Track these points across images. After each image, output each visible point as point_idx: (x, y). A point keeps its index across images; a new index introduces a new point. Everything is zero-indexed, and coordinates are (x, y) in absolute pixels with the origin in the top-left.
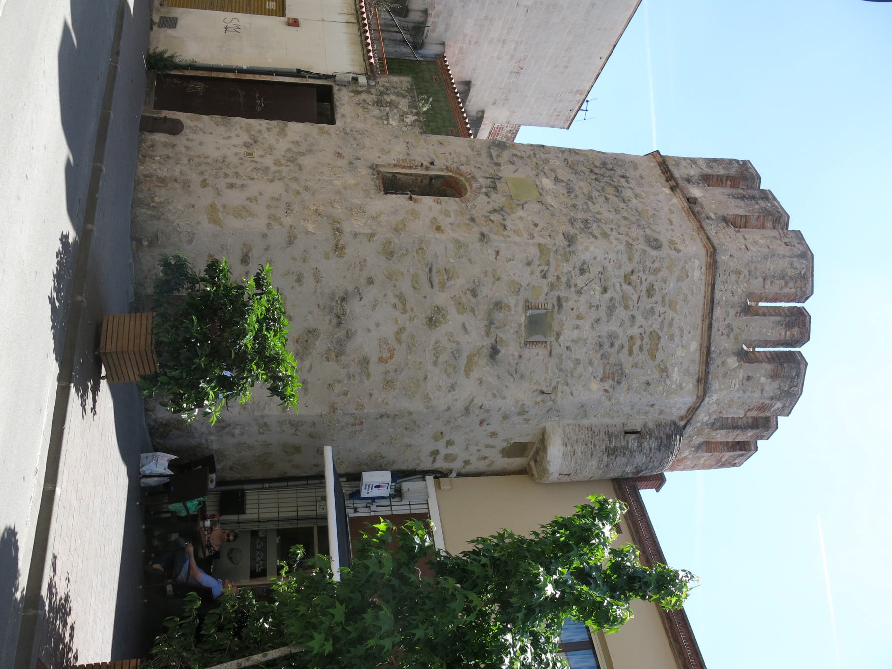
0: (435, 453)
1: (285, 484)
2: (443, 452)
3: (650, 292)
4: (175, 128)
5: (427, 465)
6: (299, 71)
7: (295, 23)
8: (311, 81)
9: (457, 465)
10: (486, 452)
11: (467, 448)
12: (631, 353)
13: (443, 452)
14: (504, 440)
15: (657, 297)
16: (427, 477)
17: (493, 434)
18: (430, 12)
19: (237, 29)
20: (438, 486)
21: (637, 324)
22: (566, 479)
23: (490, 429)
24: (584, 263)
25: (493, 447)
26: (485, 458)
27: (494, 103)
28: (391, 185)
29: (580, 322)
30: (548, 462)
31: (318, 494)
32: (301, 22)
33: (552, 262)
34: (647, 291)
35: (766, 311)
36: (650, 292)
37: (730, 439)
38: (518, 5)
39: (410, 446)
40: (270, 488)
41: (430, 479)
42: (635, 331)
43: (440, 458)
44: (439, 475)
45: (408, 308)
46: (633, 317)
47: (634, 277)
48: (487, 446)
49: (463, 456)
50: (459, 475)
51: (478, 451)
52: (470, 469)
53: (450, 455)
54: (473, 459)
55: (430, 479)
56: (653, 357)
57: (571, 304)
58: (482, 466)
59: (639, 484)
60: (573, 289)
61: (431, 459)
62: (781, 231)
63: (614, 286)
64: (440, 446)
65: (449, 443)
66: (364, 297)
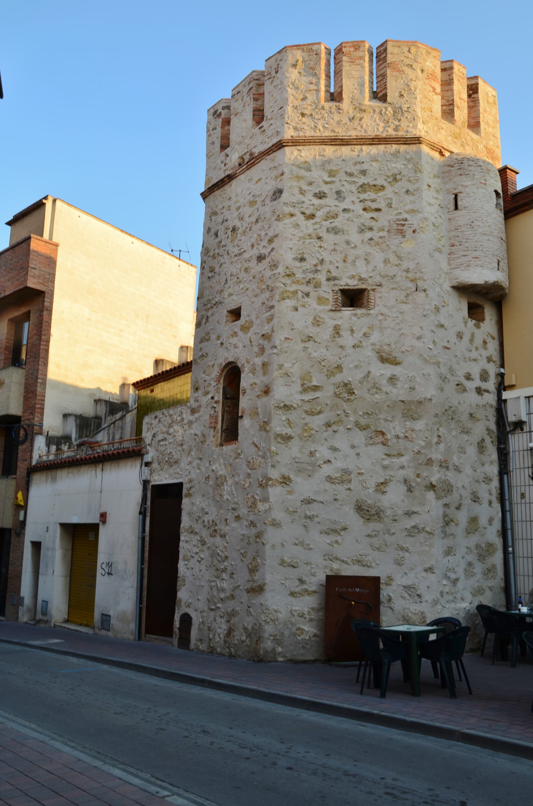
0: (479, 391)
1: (509, 532)
2: (477, 383)
3: (321, 196)
4: (186, 619)
5: (491, 399)
6: (140, 513)
7: (103, 516)
8: (149, 503)
9: (492, 370)
10: (478, 341)
11: (474, 360)
12: (378, 210)
13: (477, 383)
14: (466, 323)
15: (325, 188)
16: (503, 398)
17: (460, 336)
18: (97, 398)
19: (110, 565)
20: (512, 387)
21: (352, 207)
22: (504, 265)
23: (454, 339)
24: (295, 259)
25: (473, 335)
26: (485, 342)
27: (175, 337)
28: (231, 433)
29: (350, 259)
30: (486, 282)
31: (519, 501)
32: (102, 510)
33: (294, 287)
34: (320, 198)
35: (338, 86)
36: (321, 196)
37: (465, 105)
38: (89, 320)
39: (471, 415)
40: (513, 546)
41: (505, 395)
42: (358, 208)
43: (485, 386)
44: (502, 386)
45: (337, 419)
46: (345, 210)
47: (308, 212)
48: (472, 340)
49: (483, 364)
50: (502, 366)
51: (477, 349)
52: (496, 357)
53: (481, 376)
54: (486, 354)
55: (505, 395)
56: (383, 188)
57: (332, 268)
58: (493, 347)
59: (511, 191)
60: (319, 268)
61: (486, 394)
62: (267, 78)
63: (315, 230)
64: (471, 385)
65: (468, 377)
66: (328, 458)
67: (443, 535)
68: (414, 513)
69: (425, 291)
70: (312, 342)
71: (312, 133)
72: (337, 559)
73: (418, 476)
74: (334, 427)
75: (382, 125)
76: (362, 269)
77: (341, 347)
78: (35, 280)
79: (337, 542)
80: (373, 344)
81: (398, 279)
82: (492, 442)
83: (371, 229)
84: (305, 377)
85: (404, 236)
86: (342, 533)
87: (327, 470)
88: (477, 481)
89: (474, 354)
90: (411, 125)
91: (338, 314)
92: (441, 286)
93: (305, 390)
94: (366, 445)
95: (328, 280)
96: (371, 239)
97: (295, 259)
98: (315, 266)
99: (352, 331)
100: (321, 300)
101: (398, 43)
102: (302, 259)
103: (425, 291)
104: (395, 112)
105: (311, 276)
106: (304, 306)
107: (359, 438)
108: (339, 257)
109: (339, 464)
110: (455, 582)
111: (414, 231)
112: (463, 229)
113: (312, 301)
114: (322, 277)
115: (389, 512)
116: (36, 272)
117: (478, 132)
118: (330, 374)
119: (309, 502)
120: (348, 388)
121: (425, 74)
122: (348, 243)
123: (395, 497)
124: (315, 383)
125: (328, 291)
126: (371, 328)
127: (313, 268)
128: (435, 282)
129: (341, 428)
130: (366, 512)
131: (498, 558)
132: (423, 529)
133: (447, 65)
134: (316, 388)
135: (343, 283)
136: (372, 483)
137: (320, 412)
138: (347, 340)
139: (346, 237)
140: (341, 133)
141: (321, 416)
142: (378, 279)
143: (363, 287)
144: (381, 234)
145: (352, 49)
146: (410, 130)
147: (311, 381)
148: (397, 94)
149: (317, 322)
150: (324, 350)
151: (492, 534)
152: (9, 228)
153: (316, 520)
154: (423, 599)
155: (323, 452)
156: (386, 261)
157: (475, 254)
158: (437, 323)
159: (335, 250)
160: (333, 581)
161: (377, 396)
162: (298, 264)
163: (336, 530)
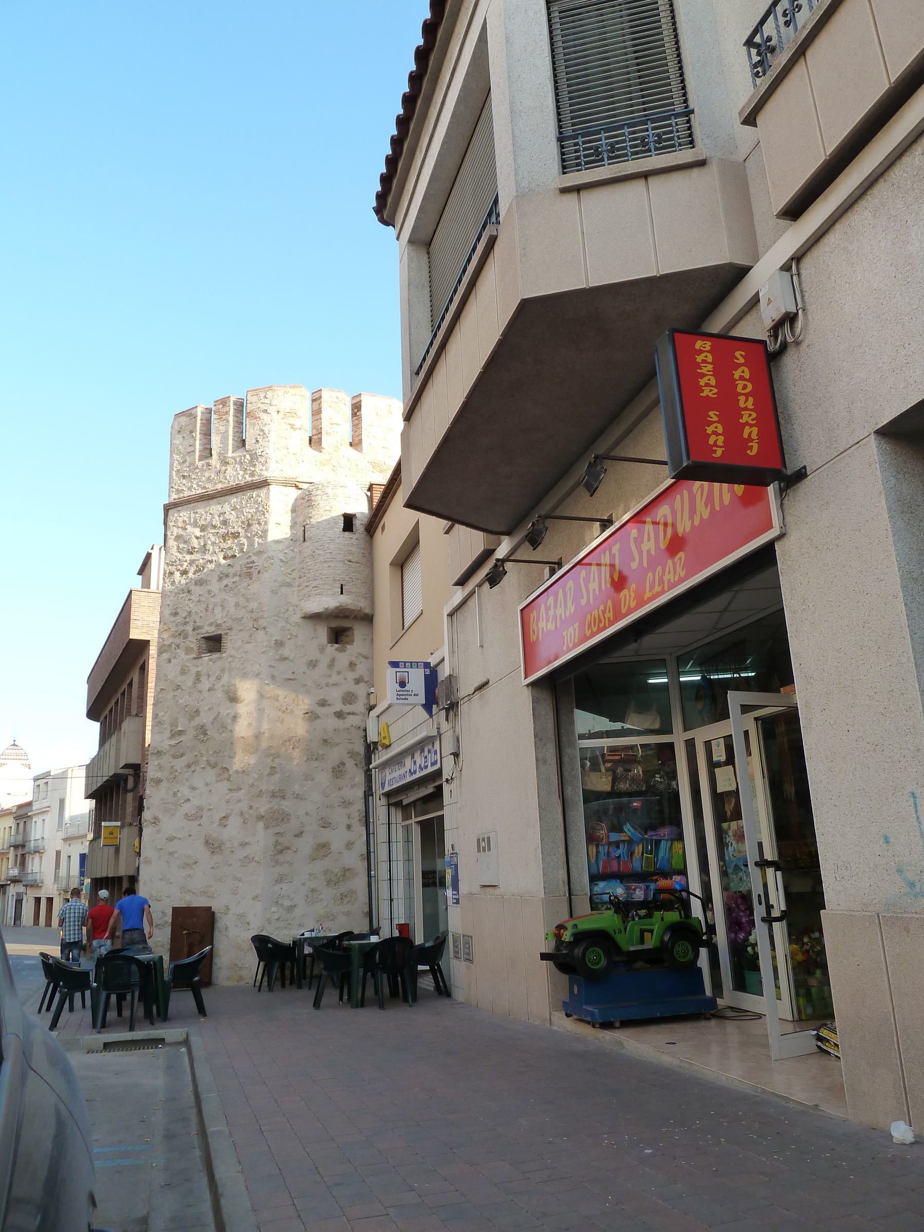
30: (327, 609)
67: (273, 863)
68: (246, 844)
69: (264, 628)
70: (179, 690)
71: (190, 493)
72: (189, 891)
73: (251, 807)
74: (193, 768)
75: (241, 473)
76: (219, 616)
77: (200, 692)
78: (138, 631)
79: (189, 875)
80: (223, 686)
81: (245, 620)
82: (356, 765)
83: (227, 576)
84: (174, 724)
85: (251, 579)
86: (194, 866)
87: (187, 808)
88: (331, 807)
89: (335, 678)
90: (264, 468)
91: (200, 661)
92: (287, 620)
93: (172, 736)
94: (217, 781)
95: (194, 630)
96: (227, 586)
97: (171, 614)
98: (185, 618)
99: (209, 676)
100: (188, 650)
101: (256, 392)
102: (176, 614)
103: (264, 628)
104: (252, 459)
105: (181, 628)
106: (175, 657)
107: (211, 775)
108: (202, 607)
109: (195, 802)
110: (291, 908)
111: (259, 572)
112: (307, 560)
113: (181, 653)
114: (189, 628)
115: (228, 845)
116: (139, 623)
117: (360, 451)
118: (192, 718)
119: (171, 839)
120: (202, 730)
121: (281, 414)
122: (209, 592)
123: (233, 832)
124: (180, 729)
125: (193, 642)
126: (223, 670)
127: (184, 621)
128: (279, 617)
129: (198, 768)
130: (213, 846)
131: (359, 883)
132: (253, 858)
133: (317, 396)
134: (181, 733)
135: (204, 631)
136: (217, 817)
137: (182, 755)
138: (205, 684)
139: (209, 587)
140: (211, 488)
141: (184, 758)
142: (230, 622)
143: (219, 632)
144: (234, 580)
145: (221, 406)
146: (263, 473)
147: (177, 727)
148: (254, 441)
149: (183, 672)
150: (187, 697)
151: (354, 859)
152: (140, 577)
153: (176, 855)
154: (251, 927)
155: (184, 791)
156: (237, 605)
157: (315, 583)
158: (278, 657)
159: (199, 601)
160: (177, 912)
161: (224, 735)
162: (173, 619)
163: (190, 864)
